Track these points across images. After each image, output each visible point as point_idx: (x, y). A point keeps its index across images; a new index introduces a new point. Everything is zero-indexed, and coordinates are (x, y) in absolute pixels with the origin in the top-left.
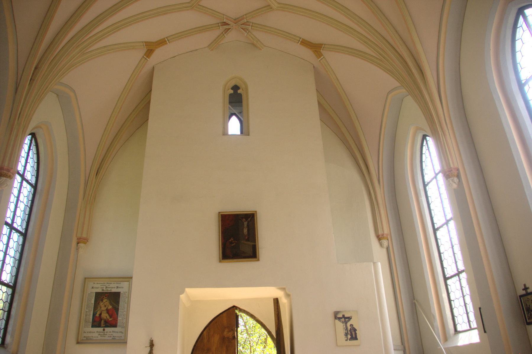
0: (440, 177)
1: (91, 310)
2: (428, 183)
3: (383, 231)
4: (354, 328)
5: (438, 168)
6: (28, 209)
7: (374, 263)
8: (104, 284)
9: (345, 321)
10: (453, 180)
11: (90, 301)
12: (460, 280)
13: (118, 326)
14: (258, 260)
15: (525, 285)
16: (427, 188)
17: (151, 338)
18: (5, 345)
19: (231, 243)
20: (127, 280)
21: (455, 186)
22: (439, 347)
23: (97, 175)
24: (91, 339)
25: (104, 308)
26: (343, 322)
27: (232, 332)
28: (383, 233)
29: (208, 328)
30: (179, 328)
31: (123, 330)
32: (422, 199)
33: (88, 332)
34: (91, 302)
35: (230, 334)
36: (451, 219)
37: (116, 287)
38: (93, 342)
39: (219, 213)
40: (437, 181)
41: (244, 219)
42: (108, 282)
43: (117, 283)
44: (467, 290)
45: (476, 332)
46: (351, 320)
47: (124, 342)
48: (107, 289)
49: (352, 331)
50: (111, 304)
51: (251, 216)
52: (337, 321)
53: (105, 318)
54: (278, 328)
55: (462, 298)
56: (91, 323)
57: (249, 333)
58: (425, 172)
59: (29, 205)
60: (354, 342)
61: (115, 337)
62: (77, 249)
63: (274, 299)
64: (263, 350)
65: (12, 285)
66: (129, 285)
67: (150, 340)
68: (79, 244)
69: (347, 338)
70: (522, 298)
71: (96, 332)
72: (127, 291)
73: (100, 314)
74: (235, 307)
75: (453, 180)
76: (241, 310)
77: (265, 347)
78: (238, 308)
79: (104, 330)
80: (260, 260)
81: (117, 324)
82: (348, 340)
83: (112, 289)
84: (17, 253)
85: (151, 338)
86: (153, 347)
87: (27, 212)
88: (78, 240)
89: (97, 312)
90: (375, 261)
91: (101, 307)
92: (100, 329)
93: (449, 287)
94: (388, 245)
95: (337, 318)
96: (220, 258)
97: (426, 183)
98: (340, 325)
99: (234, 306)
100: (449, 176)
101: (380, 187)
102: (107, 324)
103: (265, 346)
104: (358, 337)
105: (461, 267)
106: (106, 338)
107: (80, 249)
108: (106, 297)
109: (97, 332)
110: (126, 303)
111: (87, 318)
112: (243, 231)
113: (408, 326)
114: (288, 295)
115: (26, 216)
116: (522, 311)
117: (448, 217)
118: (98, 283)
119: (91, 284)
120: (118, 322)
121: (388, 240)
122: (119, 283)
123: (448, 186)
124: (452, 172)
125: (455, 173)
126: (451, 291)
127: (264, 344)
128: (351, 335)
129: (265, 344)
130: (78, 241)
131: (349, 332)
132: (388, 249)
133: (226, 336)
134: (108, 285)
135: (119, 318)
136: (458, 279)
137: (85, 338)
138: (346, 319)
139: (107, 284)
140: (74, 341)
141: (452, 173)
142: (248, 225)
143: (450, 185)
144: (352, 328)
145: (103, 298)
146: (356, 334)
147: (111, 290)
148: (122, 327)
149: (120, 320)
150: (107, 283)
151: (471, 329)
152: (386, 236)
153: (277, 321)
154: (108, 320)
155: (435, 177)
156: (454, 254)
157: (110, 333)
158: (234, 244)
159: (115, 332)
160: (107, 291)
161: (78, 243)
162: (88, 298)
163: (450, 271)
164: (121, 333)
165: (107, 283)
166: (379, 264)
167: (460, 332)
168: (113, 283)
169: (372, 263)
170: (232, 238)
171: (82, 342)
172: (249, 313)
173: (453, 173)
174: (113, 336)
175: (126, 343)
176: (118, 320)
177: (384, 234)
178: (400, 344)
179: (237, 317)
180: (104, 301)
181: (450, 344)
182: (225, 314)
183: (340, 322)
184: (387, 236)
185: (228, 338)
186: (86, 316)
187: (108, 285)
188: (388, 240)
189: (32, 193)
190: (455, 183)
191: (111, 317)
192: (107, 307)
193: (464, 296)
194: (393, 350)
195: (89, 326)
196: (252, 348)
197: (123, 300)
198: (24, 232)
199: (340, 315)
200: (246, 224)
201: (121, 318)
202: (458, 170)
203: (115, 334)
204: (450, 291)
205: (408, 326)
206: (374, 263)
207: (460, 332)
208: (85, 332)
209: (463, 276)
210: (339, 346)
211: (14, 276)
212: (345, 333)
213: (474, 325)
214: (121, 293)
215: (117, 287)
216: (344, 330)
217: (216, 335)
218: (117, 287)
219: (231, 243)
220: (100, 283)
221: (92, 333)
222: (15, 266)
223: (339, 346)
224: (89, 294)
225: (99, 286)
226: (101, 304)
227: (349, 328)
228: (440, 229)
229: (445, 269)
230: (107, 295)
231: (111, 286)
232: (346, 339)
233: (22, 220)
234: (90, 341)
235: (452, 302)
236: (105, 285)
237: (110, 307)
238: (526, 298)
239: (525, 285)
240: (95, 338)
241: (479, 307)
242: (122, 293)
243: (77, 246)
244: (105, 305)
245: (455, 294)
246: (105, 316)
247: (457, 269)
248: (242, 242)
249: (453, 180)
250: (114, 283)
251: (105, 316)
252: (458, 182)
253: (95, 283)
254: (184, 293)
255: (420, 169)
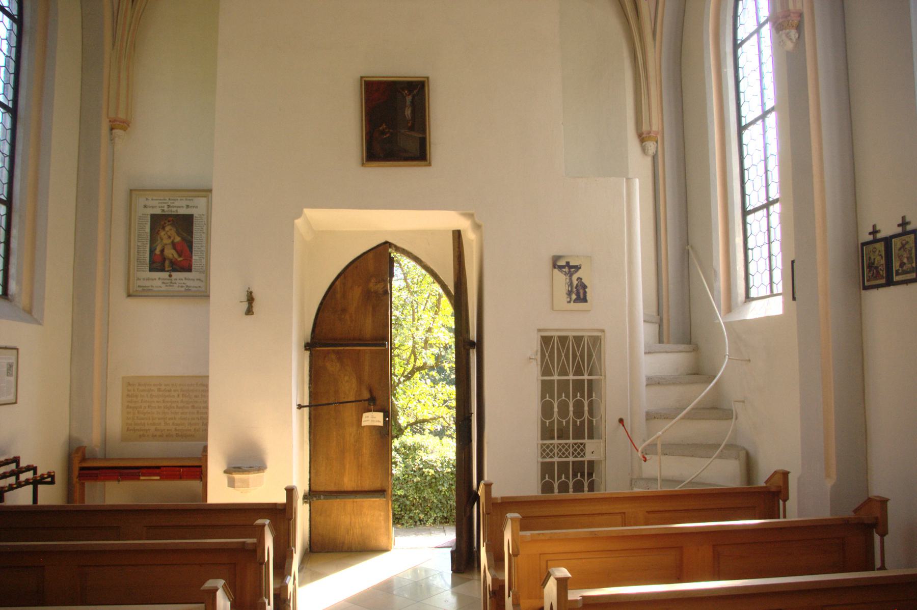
0: (766, 31)
1: (147, 244)
2: (743, 42)
3: (651, 125)
4: (583, 283)
5: (765, 13)
6: (12, 64)
7: (628, 179)
8: (165, 201)
9: (570, 271)
10: (788, 33)
11: (143, 228)
12: (768, 215)
13: (193, 270)
14: (430, 165)
15: (874, 226)
16: (740, 51)
17: (249, 288)
18: (9, 297)
19: (383, 133)
20: (204, 193)
21: (790, 46)
22: (717, 321)
23: (134, 3)
24: (150, 290)
25: (167, 241)
26: (566, 274)
27: (382, 284)
28: (649, 129)
29: (342, 277)
30: (294, 267)
31: (202, 276)
32: (726, 72)
33: (144, 279)
34: (144, 231)
35: (379, 286)
36: (772, 109)
37: (184, 206)
38: (154, 294)
39: (362, 78)
40: (759, 38)
41: (406, 92)
42: (171, 198)
43: (186, 200)
44: (777, 233)
45: (780, 299)
46: (580, 271)
47: (204, 295)
48: (170, 209)
49: (579, 287)
50: (178, 234)
51: (419, 87)
52: (556, 271)
53: (171, 256)
54: (458, 278)
55: (766, 246)
56: (148, 265)
57: (412, 290)
58: (741, 20)
59: (13, 56)
60: (581, 305)
61: (190, 287)
62: (112, 140)
63: (454, 232)
64: (433, 318)
65: (5, 199)
66: (208, 202)
67: (247, 291)
68: (114, 131)
69: (571, 298)
70: (864, 247)
71: (157, 279)
72: (205, 213)
73: (162, 251)
74: (388, 244)
75: (788, 35)
76: (398, 249)
77: (436, 313)
78: (393, 246)
79: (170, 276)
80: (432, 165)
81: (191, 266)
82: (572, 302)
83: (179, 210)
84: (4, 143)
85: (249, 288)
86: (252, 303)
87: (12, 70)
88: (111, 123)
89: (157, 246)
90: (630, 176)
91: (162, 239)
92: (165, 275)
93: (748, 226)
94: (657, 151)
95: (557, 267)
96: (363, 159)
97: (739, 42)
98: (560, 278)
99: (386, 243)
100: (783, 26)
101: (655, 45)
102: (174, 267)
103: (436, 311)
104: (588, 298)
105: (774, 194)
106: (176, 288)
107: (117, 139)
108: (169, 223)
109: (159, 279)
110: (204, 233)
111: (140, 256)
112: (405, 113)
113: (671, 287)
114: (477, 227)
115: (10, 77)
116: (861, 278)
117: (768, 107)
118: (154, 198)
119: (141, 201)
120: (193, 263)
121: (657, 142)
122: (190, 200)
123: (777, 45)
124: (789, 18)
125: (795, 20)
126: (753, 285)
127: (436, 308)
128: (578, 294)
129: (437, 308)
130: (111, 125)
131: (574, 290)
132: (654, 157)
133: (372, 290)
134: (171, 203)
135: (194, 257)
136: (765, 215)
137: (141, 289)
138: (571, 269)
139: (170, 201)
140: (123, 294)
141: (788, 21)
142: (413, 102)
143: (782, 44)
144: (579, 284)
145: (165, 223)
146: (585, 293)
147: (177, 211)
148: (200, 272)
149: (197, 260)
150: (169, 199)
151: (772, 295)
152: (655, 135)
153: (457, 267)
154: (176, 259)
155: (757, 31)
156: (766, 171)
157: (182, 282)
158: (388, 135)
159: (189, 279)
160: (170, 213)
161: (112, 129)
162: (139, 224)
163: (753, 201)
164: (198, 281)
165: (169, 199)
166: (637, 182)
167: (754, 299)
168: (179, 199)
169: (625, 179)
170: (384, 125)
171: (134, 294)
172: (411, 253)
173: (791, 21)
174: (187, 286)
175: (209, 296)
176: (193, 261)
177: (652, 132)
178: (655, 314)
179: (391, 261)
180: (167, 228)
181: (735, 317)
182: (371, 255)
183: (561, 273)
184: (656, 134)
185: (376, 292)
186: (139, 253)
187: (171, 203)
188: (657, 142)
189: (16, 32)
190: (791, 39)
191: (180, 256)
192: (172, 239)
193: (769, 243)
194: (643, 322)
195: (145, 269)
196: (416, 314)
197: (198, 227)
198: (10, 106)
199: (562, 263)
200: (409, 99)
201: (197, 257)
202: (801, 15)
203: (189, 283)
204: (749, 233)
205: (671, 287)
206: (628, 179)
207: (754, 299)
208: (139, 279)
209: (776, 209)
210: (555, 310)
211: (6, 184)
212: (568, 290)
213: (778, 288)
214: (194, 216)
215: (188, 206)
216: (566, 286)
217: (357, 286)
218: (188, 206)
219: (383, 133)
220: (157, 200)
221: (151, 281)
222: (5, 166)
223: (555, 310)
224: (140, 217)
225: (155, 203)
226: (162, 233)
227: (575, 283)
228: (750, 128)
229: (747, 197)
230: (170, 219)
231: (177, 203)
232: (569, 300)
233: (5, 84)
234: (150, 294)
235: (750, 252)
236: (166, 203)
237: (178, 239)
238: (871, 247)
239: (874, 226)
240: (155, 289)
241: (793, 259)
242: (196, 217)
243: (111, 134)
244: (169, 235)
245: (757, 238)
246: (170, 253)
247: (768, 197)
248: (403, 131)
249: (788, 33)
250: (181, 200)
251: (170, 253)
252: (796, 40)
253: (149, 200)
254: (303, 216)
255: (732, 14)
